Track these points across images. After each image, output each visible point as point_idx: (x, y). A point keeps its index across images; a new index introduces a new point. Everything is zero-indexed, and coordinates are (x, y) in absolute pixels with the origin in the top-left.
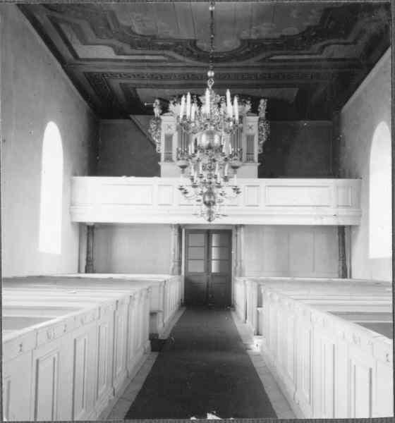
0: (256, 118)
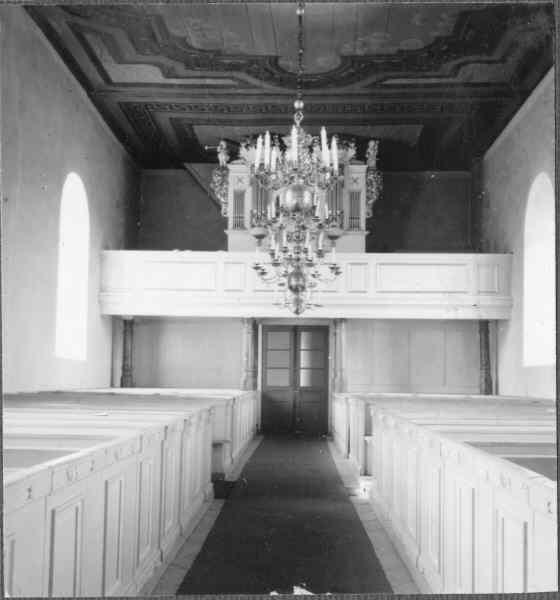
0: (363, 168)
